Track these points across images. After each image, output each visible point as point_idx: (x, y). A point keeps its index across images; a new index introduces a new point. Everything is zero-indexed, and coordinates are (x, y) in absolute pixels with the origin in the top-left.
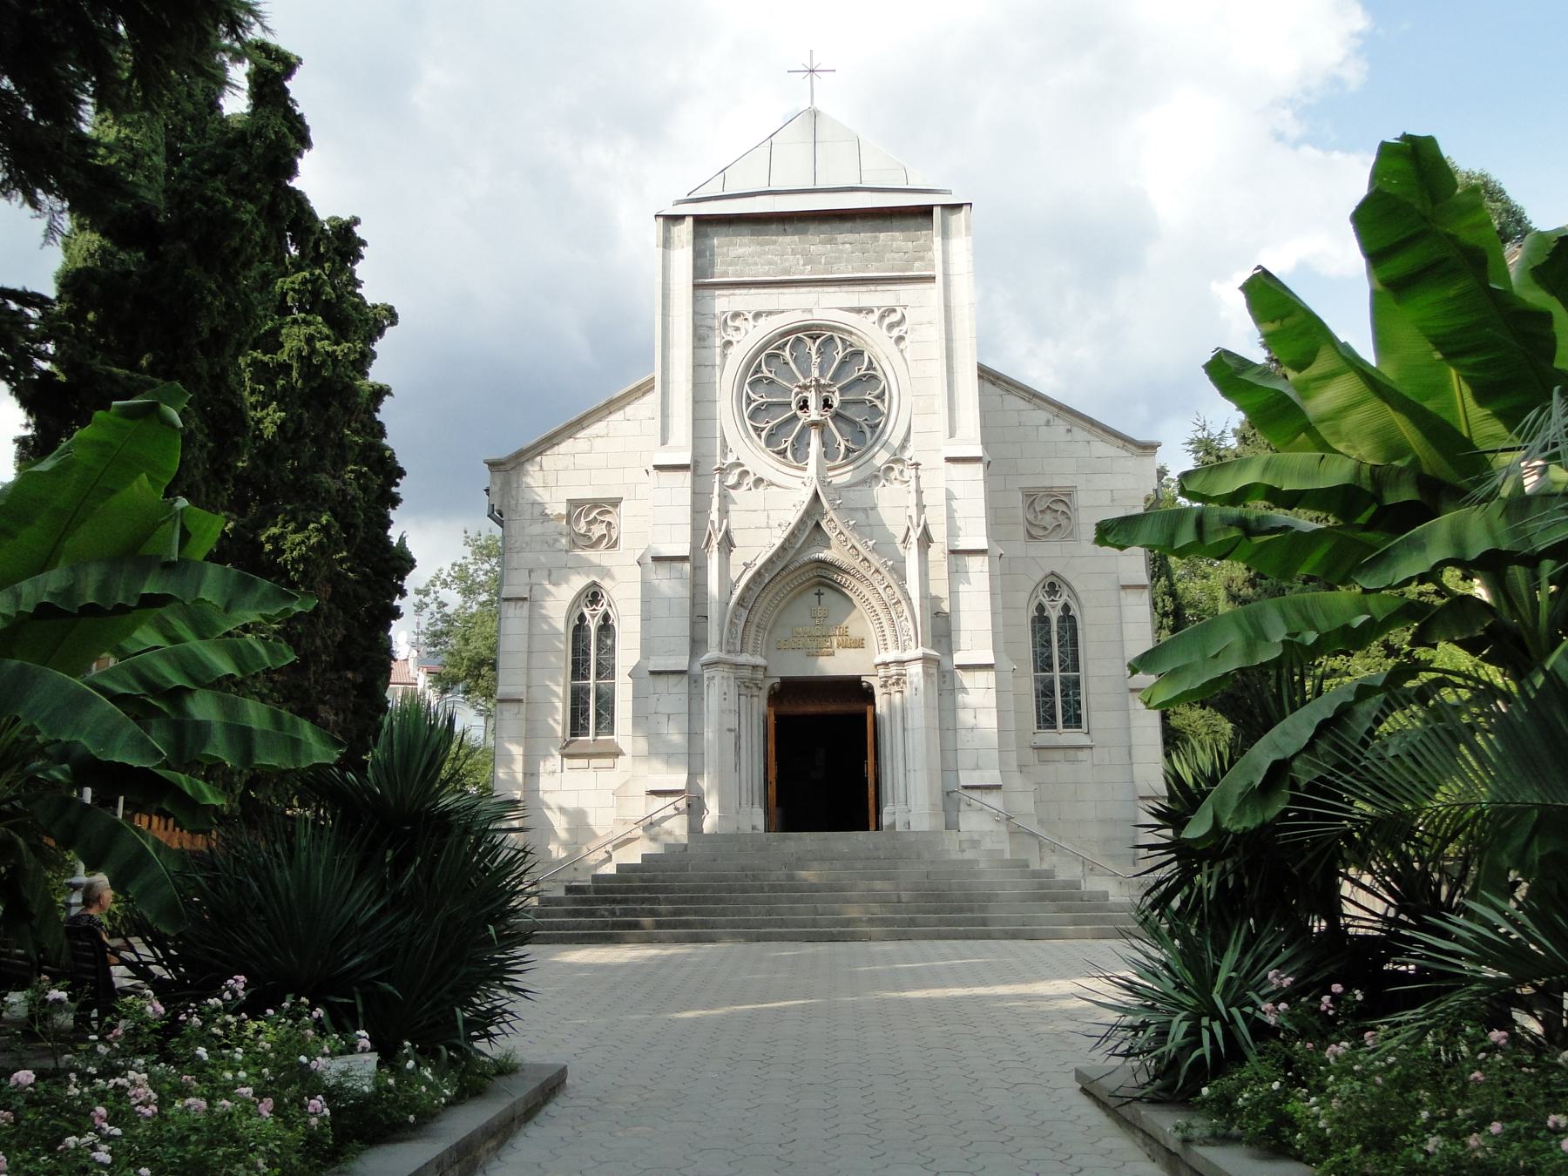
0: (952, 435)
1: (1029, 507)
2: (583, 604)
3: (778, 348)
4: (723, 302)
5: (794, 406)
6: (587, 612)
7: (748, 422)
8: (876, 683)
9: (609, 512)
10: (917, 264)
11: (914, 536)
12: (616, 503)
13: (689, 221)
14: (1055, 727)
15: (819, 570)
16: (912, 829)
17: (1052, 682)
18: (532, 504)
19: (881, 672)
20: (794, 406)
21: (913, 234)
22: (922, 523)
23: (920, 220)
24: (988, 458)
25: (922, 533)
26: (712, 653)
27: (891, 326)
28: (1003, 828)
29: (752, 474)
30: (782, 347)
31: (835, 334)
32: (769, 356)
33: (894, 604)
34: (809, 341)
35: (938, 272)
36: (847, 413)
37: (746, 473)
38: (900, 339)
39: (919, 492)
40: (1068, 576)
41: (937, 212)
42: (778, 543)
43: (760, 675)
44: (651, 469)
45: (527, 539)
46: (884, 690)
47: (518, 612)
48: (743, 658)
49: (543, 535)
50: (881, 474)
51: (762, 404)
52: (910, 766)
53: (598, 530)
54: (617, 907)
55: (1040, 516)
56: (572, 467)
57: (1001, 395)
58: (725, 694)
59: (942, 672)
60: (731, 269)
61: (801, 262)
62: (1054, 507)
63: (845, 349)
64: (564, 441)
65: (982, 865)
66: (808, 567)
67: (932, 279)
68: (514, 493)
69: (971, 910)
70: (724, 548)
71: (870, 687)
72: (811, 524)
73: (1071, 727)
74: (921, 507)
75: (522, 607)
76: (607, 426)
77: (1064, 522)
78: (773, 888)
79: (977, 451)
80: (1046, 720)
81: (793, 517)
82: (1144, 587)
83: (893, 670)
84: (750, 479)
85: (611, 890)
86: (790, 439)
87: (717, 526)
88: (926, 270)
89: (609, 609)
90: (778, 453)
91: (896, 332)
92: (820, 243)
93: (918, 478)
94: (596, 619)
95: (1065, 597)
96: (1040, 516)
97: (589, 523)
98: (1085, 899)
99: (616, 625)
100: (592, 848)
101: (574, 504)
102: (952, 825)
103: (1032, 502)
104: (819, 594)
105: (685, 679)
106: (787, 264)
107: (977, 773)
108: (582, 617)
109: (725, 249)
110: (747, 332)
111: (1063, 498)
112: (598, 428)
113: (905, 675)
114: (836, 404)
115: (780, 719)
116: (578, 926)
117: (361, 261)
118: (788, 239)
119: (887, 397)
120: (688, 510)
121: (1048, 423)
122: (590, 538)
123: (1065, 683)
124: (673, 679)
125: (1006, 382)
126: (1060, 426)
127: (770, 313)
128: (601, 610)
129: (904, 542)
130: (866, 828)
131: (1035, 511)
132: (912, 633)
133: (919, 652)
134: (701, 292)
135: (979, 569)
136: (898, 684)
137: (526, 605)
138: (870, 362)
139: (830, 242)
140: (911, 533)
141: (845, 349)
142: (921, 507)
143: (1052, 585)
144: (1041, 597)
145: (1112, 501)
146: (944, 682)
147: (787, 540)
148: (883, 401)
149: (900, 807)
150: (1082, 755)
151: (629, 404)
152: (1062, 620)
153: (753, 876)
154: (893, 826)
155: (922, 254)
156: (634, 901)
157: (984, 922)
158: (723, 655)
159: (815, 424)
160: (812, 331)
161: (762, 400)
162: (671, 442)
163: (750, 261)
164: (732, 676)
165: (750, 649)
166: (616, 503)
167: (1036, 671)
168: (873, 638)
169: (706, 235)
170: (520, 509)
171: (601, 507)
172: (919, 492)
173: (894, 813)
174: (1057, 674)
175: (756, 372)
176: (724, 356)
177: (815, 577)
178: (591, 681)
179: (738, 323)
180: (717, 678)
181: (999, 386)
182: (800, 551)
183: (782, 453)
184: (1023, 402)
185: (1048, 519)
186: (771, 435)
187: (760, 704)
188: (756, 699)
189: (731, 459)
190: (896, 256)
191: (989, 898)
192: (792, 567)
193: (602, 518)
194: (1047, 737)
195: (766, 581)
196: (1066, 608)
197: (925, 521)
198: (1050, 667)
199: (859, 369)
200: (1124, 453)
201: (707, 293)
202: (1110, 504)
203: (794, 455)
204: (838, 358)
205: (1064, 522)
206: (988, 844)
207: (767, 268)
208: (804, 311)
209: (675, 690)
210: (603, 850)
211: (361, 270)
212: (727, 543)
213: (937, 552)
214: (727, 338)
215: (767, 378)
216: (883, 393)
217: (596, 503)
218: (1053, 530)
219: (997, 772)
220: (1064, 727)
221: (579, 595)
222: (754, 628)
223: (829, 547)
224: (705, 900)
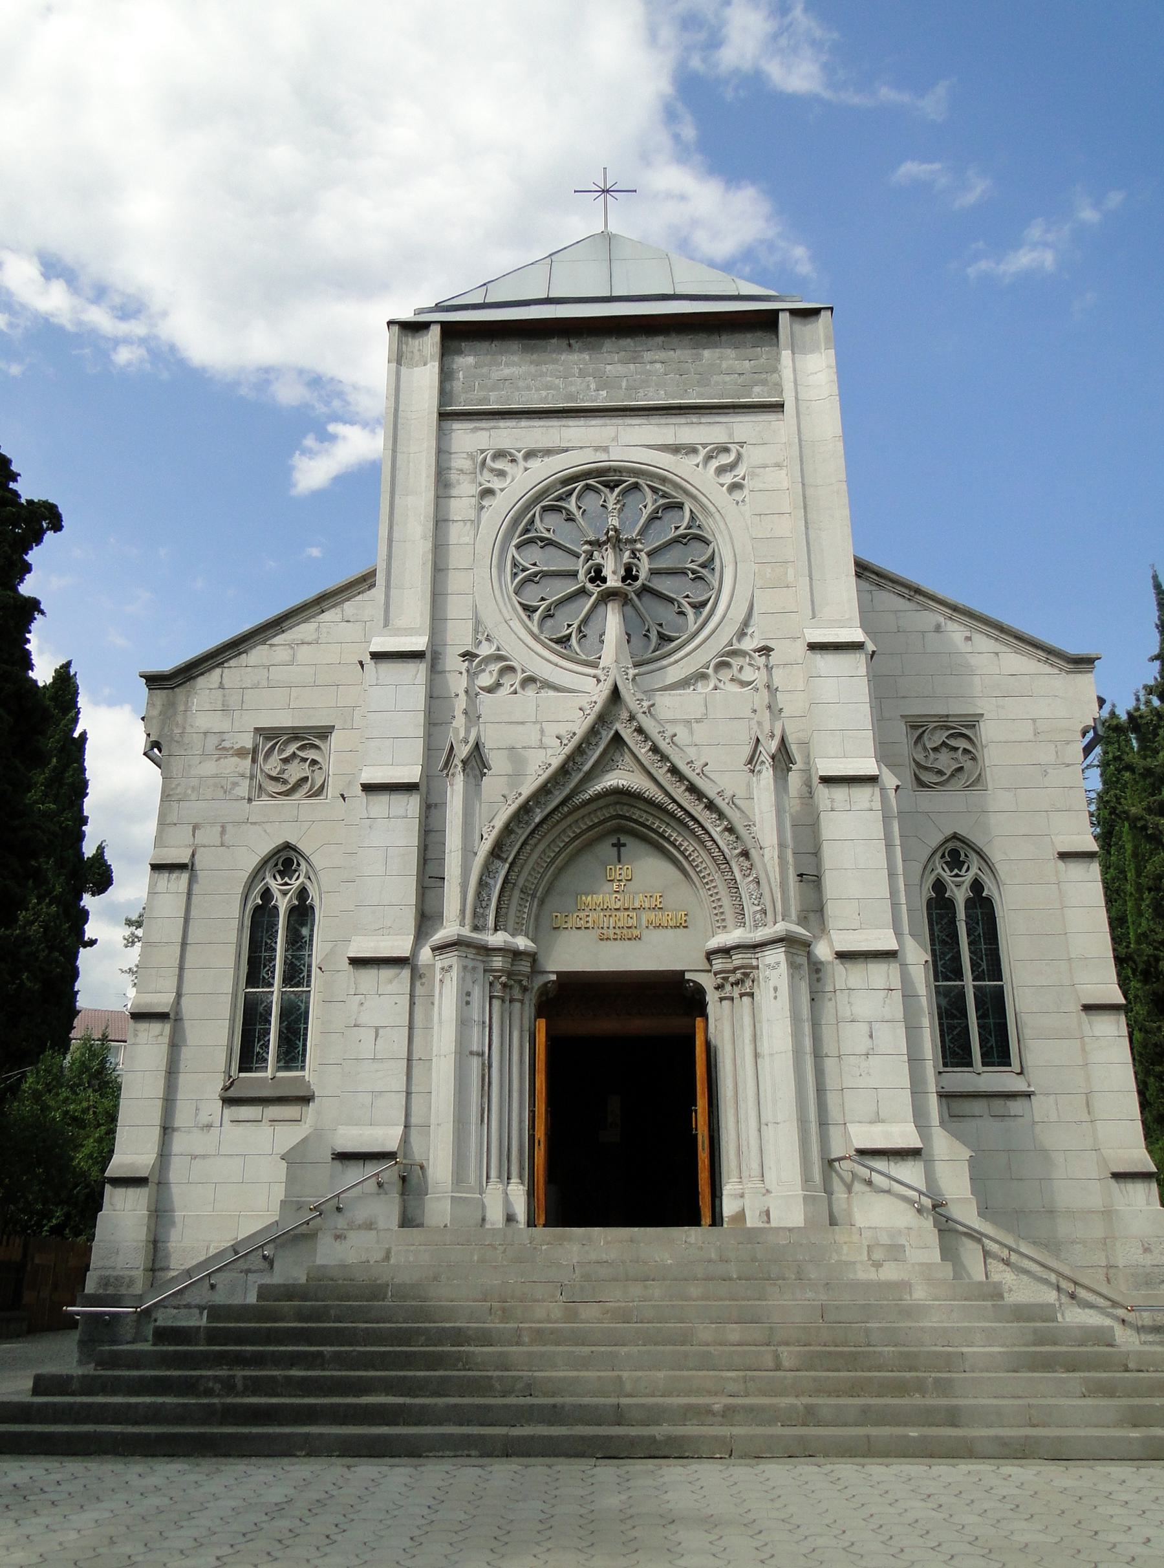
1: (916, 743)
5: (581, 576)
6: (274, 885)
7: (514, 598)
10: (757, 389)
12: (324, 733)
13: (436, 331)
14: (970, 1064)
15: (618, 807)
16: (774, 1224)
17: (961, 995)
18: (205, 733)
20: (581, 576)
21: (749, 352)
23: (759, 334)
24: (870, 647)
26: (450, 929)
28: (928, 1223)
29: (519, 671)
32: (545, 509)
37: (511, 669)
38: (735, 487)
41: (784, 318)
43: (525, 967)
44: (367, 659)
45: (194, 782)
47: (173, 886)
48: (497, 939)
49: (216, 776)
50: (710, 671)
51: (535, 574)
52: (767, 1115)
53: (295, 772)
54: (240, 1373)
56: (264, 683)
60: (493, 395)
61: (593, 386)
62: (953, 742)
63: (656, 501)
64: (255, 647)
65: (920, 1294)
66: (601, 803)
67: (779, 407)
68: (179, 718)
69: (920, 1388)
71: (700, 991)
73: (993, 1065)
77: (968, 764)
78: (539, 1336)
80: (954, 1054)
82: (1089, 856)
85: (241, 1337)
90: (559, 641)
91: (728, 479)
92: (621, 362)
95: (974, 870)
96: (932, 755)
97: (286, 761)
98: (1131, 1365)
99: (316, 904)
104: (619, 845)
105: (406, 973)
106: (573, 389)
107: (878, 1128)
108: (267, 894)
109: (485, 370)
111: (965, 731)
114: (643, 575)
115: (555, 1044)
116: (154, 1415)
118: (574, 357)
120: (421, 717)
122: (285, 782)
123: (981, 996)
124: (387, 973)
125: (877, 574)
127: (548, 452)
128: (295, 884)
129: (750, 762)
130: (695, 1221)
131: (925, 749)
135: (867, 805)
137: (185, 876)
139: (634, 361)
144: (940, 870)
145: (1036, 733)
147: (570, 758)
150: (1016, 1106)
151: (348, 599)
152: (969, 903)
153: (504, 1310)
154: (740, 1216)
155: (764, 376)
156: (278, 1360)
157: (953, 1418)
158: (466, 932)
161: (535, 569)
163: (521, 384)
164: (481, 966)
165: (511, 923)
166: (324, 733)
167: (936, 980)
170: (186, 740)
171: (304, 739)
173: (742, 1196)
174: (969, 983)
175: (526, 531)
178: (276, 988)
180: (455, 968)
182: (589, 777)
184: (902, 601)
185: (944, 761)
186: (548, 615)
188: (517, 1005)
190: (727, 378)
191: (949, 1362)
192: (578, 800)
195: (537, 820)
196: (977, 886)
197: (783, 731)
198: (959, 975)
199: (677, 528)
200: (1047, 669)
202: (1031, 737)
204: (646, 513)
205: (968, 764)
207: (544, 393)
208: (597, 449)
209: (390, 988)
210: (260, 1252)
212: (477, 763)
217: (295, 734)
218: (952, 775)
219: (911, 1127)
220: (983, 1065)
221: (265, 862)
222: (517, 894)
224: (409, 1361)
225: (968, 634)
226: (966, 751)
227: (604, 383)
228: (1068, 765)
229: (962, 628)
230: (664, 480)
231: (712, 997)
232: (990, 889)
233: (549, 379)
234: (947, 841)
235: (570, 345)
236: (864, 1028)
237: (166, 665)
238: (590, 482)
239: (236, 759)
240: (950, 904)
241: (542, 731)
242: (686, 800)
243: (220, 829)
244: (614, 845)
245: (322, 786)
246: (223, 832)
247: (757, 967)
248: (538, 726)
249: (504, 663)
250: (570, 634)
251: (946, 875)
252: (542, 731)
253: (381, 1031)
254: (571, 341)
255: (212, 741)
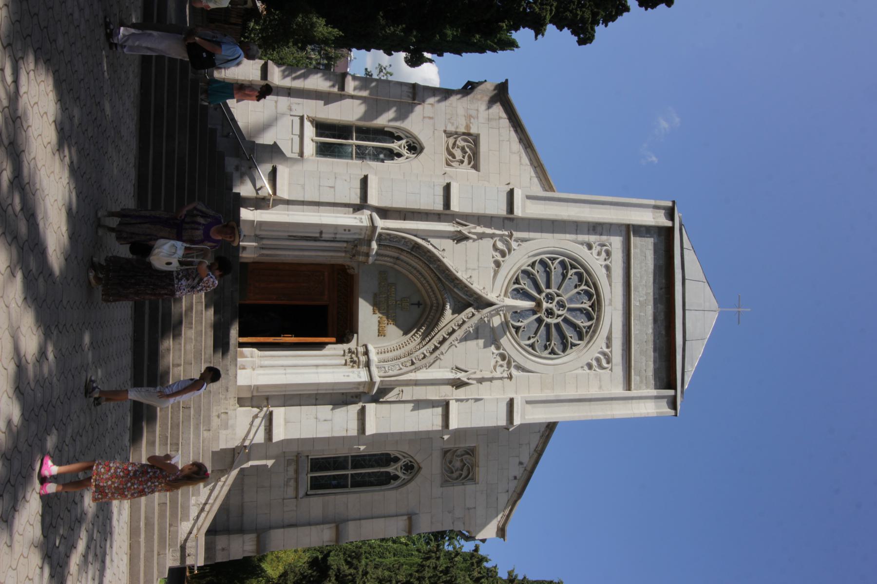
0: (528, 402)
1: (465, 451)
2: (408, 140)
3: (587, 281)
4: (616, 243)
6: (403, 142)
7: (538, 258)
8: (352, 345)
9: (469, 163)
10: (638, 378)
11: (462, 376)
12: (476, 167)
13: (669, 224)
14: (312, 471)
16: (239, 372)
18: (477, 110)
19: (361, 350)
20: (548, 291)
22: (470, 381)
25: (463, 381)
27: (598, 360)
30: (587, 284)
31: (594, 321)
33: (412, 360)
34: (590, 303)
35: (634, 393)
36: (542, 328)
39: (491, 380)
40: (419, 479)
41: (671, 392)
42: (459, 275)
43: (361, 258)
44: (511, 187)
46: (347, 351)
48: (374, 245)
49: (457, 115)
51: (550, 269)
53: (458, 153)
55: (459, 459)
57: (539, 432)
58: (349, 230)
59: (360, 395)
60: (638, 251)
61: (641, 299)
62: (465, 468)
70: (456, 236)
71: (348, 341)
72: (471, 300)
74: (481, 381)
75: (409, 96)
76: (527, 165)
77: (455, 475)
79: (517, 421)
81: (477, 287)
83: (363, 359)
84: (499, 258)
86: (526, 287)
87: (473, 231)
88: (634, 384)
89: (405, 157)
90: (517, 279)
91: (594, 363)
93: (501, 378)
94: (398, 148)
95: (403, 477)
99: (394, 161)
100: (251, 438)
101: (476, 139)
102: (241, 402)
103: (468, 454)
106: (640, 289)
107: (282, 422)
108: (399, 138)
110: (597, 259)
112: (525, 160)
113: (359, 367)
117: (625, 14)
119: (553, 356)
121: (521, 463)
122: (453, 148)
126: (518, 471)
131: (462, 455)
132: (391, 373)
133: (377, 379)
134: (624, 229)
136: (351, 362)
138: (575, 345)
140: (463, 374)
141: (584, 327)
142: (481, 381)
143: (412, 467)
144: (404, 460)
145: (469, 509)
146: (352, 397)
148: (550, 353)
149: (257, 361)
155: (644, 381)
159: (539, 304)
160: (597, 305)
162: (528, 202)
166: (476, 167)
168: (385, 343)
169: (659, 235)
172: (491, 380)
173: (252, 357)
174: (350, 472)
175: (571, 265)
176: (582, 244)
177: (432, 306)
179: (604, 254)
181: (546, 430)
183: (517, 281)
187: (340, 258)
189: (514, 245)
190: (644, 364)
193: (466, 157)
194: (307, 466)
195: (431, 266)
196: (396, 478)
197: (471, 384)
198: (354, 467)
201: (624, 233)
203: (516, 290)
204: (578, 322)
205: (455, 475)
206: (223, 434)
207: (639, 275)
208: (611, 300)
211: (611, 22)
212: (460, 238)
213: (446, 392)
214: (594, 246)
215: (567, 272)
216: (534, 349)
218: (450, 468)
221: (415, 138)
223: (453, 313)
225: (518, 478)
226: (461, 475)
227: (643, 305)
228: (453, 523)
229: (521, 475)
230: (594, 332)
231: (345, 346)
232: (394, 484)
233: (645, 278)
234: (418, 464)
235: (661, 289)
236: (329, 417)
237: (513, 94)
238: (595, 297)
239: (464, 124)
240: (387, 464)
241: (474, 269)
242: (439, 337)
243: (431, 116)
244: (419, 302)
245: (451, 166)
246: (430, 118)
247: (359, 367)
248: (477, 268)
249: (507, 251)
250: (521, 284)
251: (401, 463)
252: (474, 269)
253: (333, 189)
254: (663, 290)
255: (474, 113)
